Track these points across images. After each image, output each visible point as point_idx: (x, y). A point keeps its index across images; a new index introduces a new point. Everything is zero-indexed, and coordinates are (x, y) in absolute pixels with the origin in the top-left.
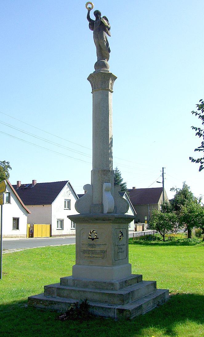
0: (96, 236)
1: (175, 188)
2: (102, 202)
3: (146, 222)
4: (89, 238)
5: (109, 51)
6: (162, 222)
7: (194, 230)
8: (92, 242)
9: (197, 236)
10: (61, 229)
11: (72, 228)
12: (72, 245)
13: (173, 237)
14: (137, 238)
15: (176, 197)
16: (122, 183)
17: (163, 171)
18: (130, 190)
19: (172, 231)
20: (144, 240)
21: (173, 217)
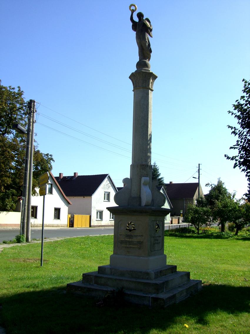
0: (133, 227)
1: (210, 184)
2: (140, 195)
3: (182, 215)
4: (127, 229)
6: (197, 216)
7: (227, 225)
8: (129, 233)
9: (230, 230)
11: (110, 220)
13: (207, 230)
14: (172, 230)
16: (160, 177)
19: (206, 225)
20: (179, 232)
21: (207, 211)
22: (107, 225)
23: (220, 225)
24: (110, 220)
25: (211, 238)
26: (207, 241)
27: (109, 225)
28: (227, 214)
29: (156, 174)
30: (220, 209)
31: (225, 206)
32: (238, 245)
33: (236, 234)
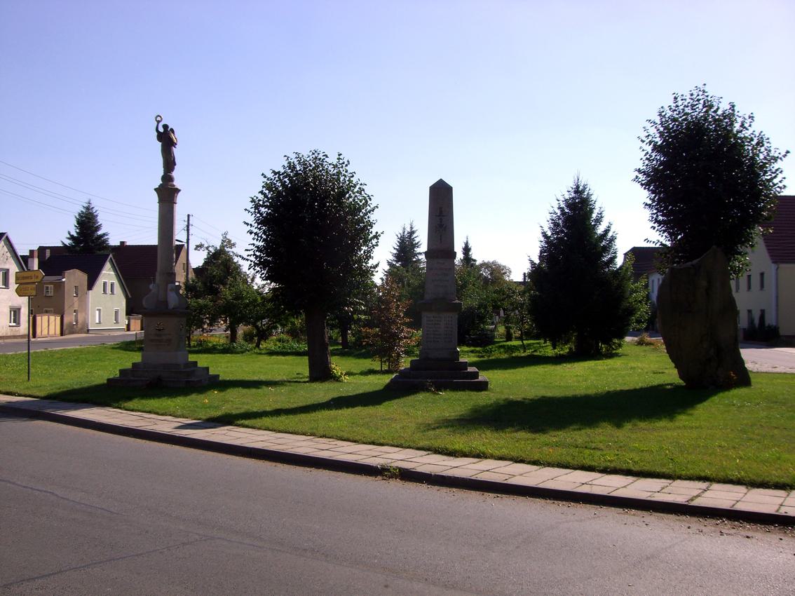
1: (206, 245)
2: (167, 298)
5: (175, 165)
7: (242, 330)
9: (246, 340)
10: (14, 324)
11: (11, 324)
12: (56, 352)
13: (205, 341)
15: (206, 263)
16: (99, 233)
17: (188, 220)
18: (115, 249)
19: (203, 331)
21: (206, 306)
22: (4, 335)
23: (229, 332)
24: (10, 326)
25: (215, 353)
26: (207, 358)
27: (9, 334)
28: (241, 311)
29: (93, 226)
30: (228, 302)
31: (238, 297)
32: (258, 361)
33: (258, 346)
